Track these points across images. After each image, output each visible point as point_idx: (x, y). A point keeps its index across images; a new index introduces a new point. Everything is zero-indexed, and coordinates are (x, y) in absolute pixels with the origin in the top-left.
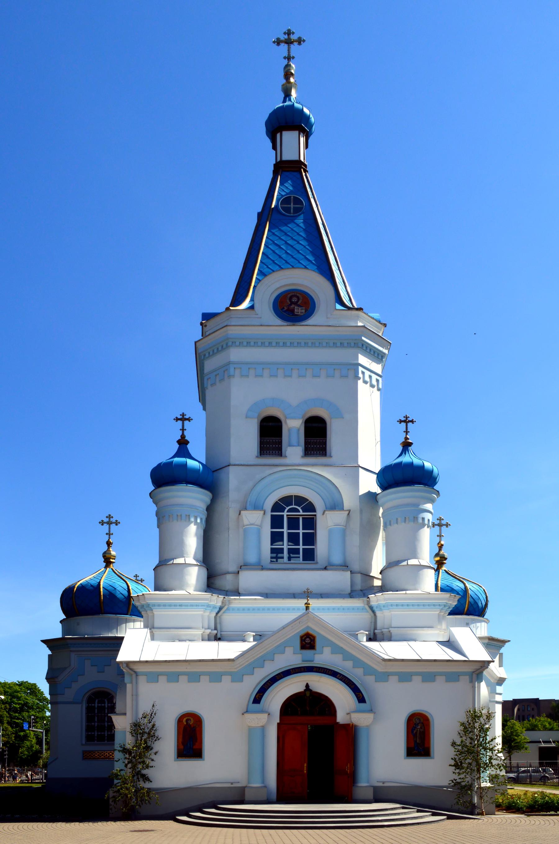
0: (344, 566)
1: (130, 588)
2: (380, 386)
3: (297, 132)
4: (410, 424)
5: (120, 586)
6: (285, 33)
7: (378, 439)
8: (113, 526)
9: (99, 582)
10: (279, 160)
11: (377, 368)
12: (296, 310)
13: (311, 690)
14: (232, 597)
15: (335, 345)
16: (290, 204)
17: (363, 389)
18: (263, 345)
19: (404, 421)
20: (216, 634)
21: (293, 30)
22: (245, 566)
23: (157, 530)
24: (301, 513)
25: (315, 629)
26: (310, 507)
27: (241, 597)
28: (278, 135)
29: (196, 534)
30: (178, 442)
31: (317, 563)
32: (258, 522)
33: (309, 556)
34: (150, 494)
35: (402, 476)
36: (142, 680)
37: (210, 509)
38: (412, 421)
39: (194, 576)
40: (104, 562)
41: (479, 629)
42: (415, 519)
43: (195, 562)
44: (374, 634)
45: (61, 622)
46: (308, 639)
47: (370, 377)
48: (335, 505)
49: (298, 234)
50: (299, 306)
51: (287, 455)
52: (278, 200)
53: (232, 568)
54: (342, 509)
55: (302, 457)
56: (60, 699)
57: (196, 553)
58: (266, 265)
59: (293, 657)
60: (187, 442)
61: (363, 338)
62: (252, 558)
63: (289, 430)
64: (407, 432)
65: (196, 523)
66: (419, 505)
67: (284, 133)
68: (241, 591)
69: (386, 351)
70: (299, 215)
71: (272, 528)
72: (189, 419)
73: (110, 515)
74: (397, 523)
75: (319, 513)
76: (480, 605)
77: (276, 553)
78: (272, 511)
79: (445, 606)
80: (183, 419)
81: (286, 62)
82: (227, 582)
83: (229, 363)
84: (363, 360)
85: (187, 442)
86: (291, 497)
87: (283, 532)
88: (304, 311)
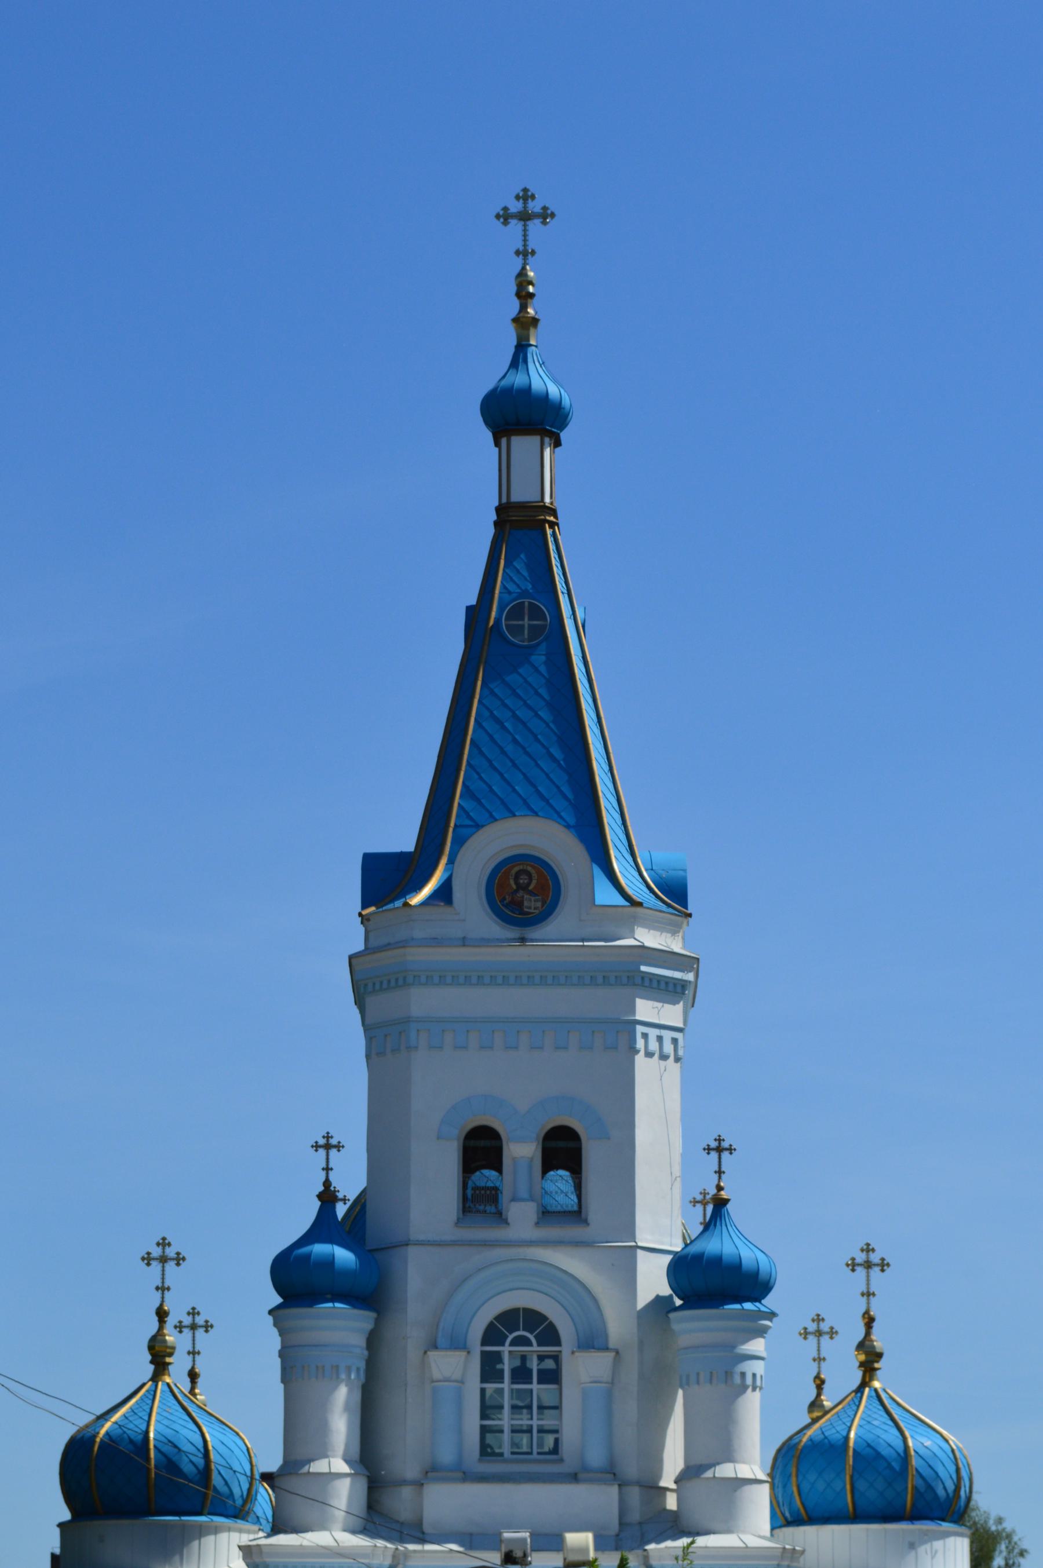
0: (611, 1473)
1: (210, 1448)
3: (536, 440)
5: (187, 1435)
7: (677, 1170)
9: (147, 1432)
11: (671, 1014)
12: (526, 904)
14: (411, 1547)
15: (593, 982)
16: (523, 620)
17: (644, 1068)
18: (467, 981)
22: (433, 1472)
23: (281, 1387)
24: (535, 1347)
26: (550, 1335)
27: (429, 1547)
29: (347, 1408)
30: (320, 1196)
31: (562, 1460)
32: (457, 1375)
35: (715, 1282)
37: (373, 1341)
38: (731, 1150)
39: (344, 1495)
40: (152, 1362)
41: (940, 1555)
42: (728, 1375)
43: (345, 1469)
45: (61, 1525)
47: (660, 1039)
48: (593, 1340)
49: (537, 693)
50: (531, 893)
51: (509, 1220)
52: (501, 609)
53: (411, 1471)
54: (606, 1349)
55: (537, 1224)
57: (347, 1446)
58: (478, 774)
61: (643, 968)
62: (446, 1455)
63: (514, 1159)
65: (349, 1382)
66: (734, 1347)
68: (427, 1528)
69: (690, 977)
70: (538, 644)
72: (339, 1147)
74: (698, 1383)
75: (566, 1348)
76: (941, 1492)
77: (486, 1451)
78: (483, 1344)
80: (328, 1145)
81: (519, 260)
82: (401, 1503)
83: (407, 1020)
84: (645, 1009)
87: (503, 1389)
88: (539, 904)
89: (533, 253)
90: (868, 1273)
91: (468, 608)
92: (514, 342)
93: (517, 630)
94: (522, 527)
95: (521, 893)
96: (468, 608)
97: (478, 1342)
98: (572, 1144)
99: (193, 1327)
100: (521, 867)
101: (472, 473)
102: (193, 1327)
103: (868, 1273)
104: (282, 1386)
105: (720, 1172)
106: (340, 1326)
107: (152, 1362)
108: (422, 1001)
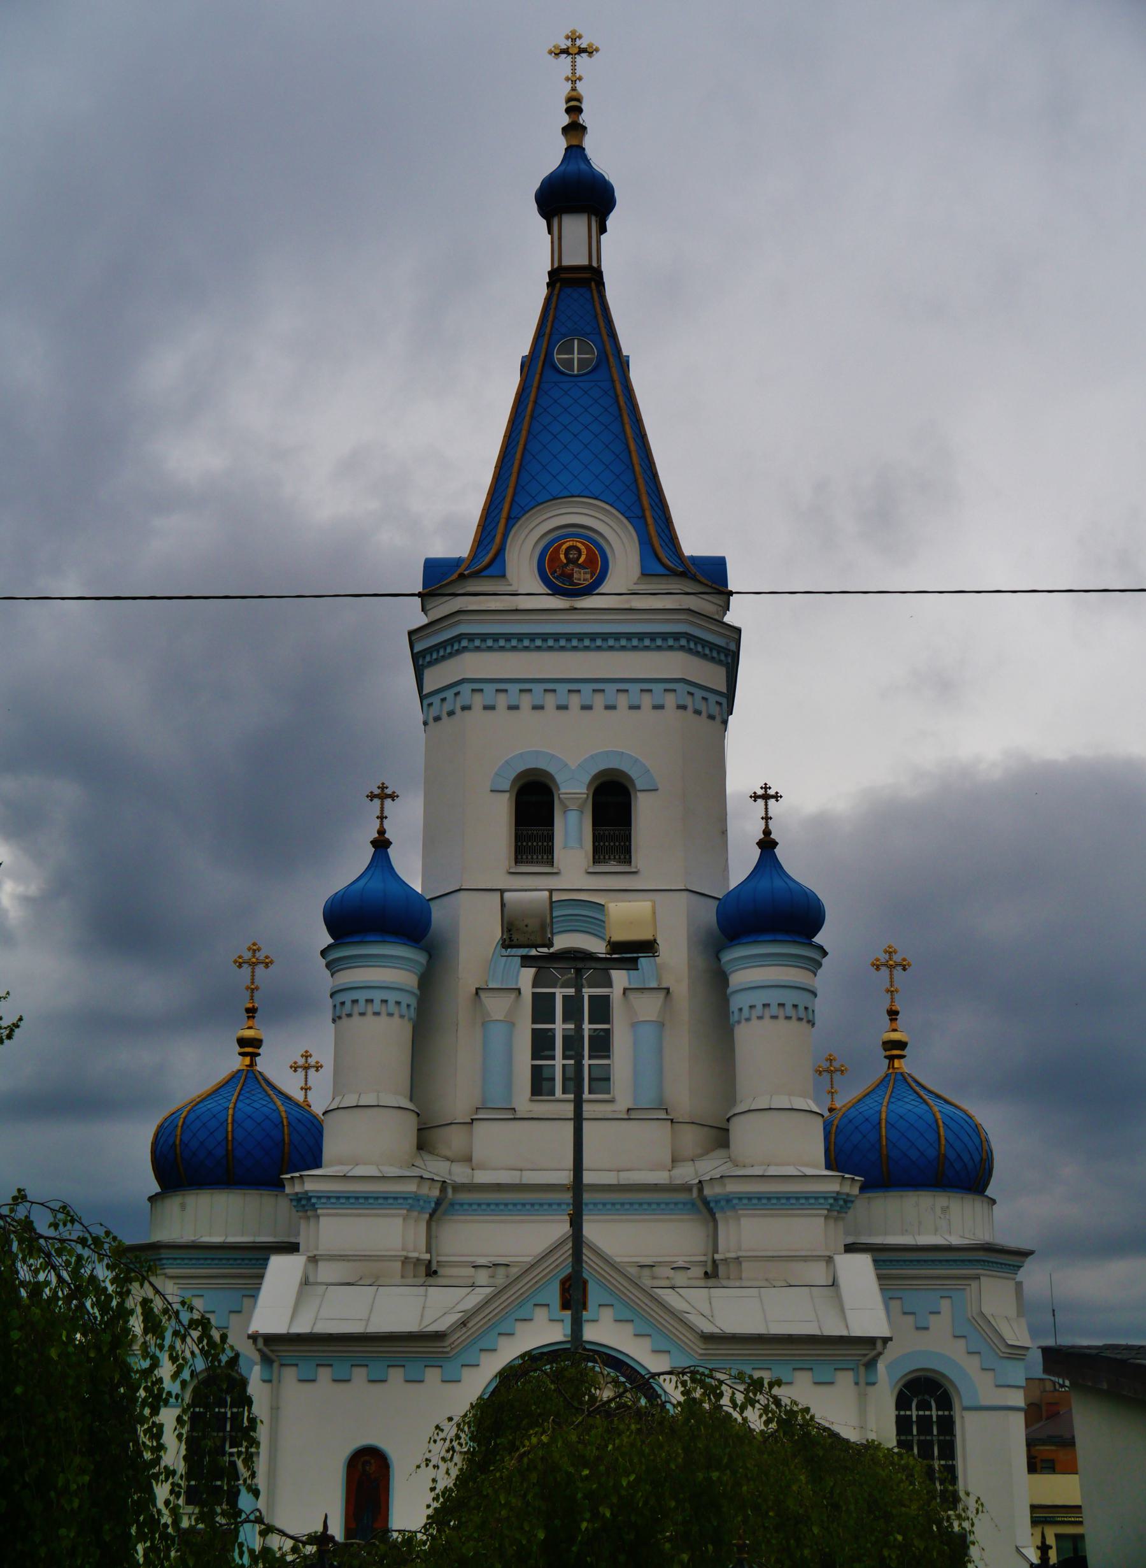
6: (567, 37)
8: (260, 969)
10: (556, 265)
12: (575, 576)
20: (430, 1261)
21: (579, 31)
50: (581, 566)
60: (774, 844)
71: (534, 1022)
77: (540, 1084)
79: (836, 1199)
85: (774, 844)
88: (588, 576)
90: (575, 152)
91: (776, 844)
94: (576, 290)
95: (571, 566)
96: (776, 844)
97: (530, 983)
99: (306, 1068)
100: (571, 543)
101: (529, 253)
102: (306, 1068)
103: (575, 152)
106: (388, 970)
108: (474, 665)
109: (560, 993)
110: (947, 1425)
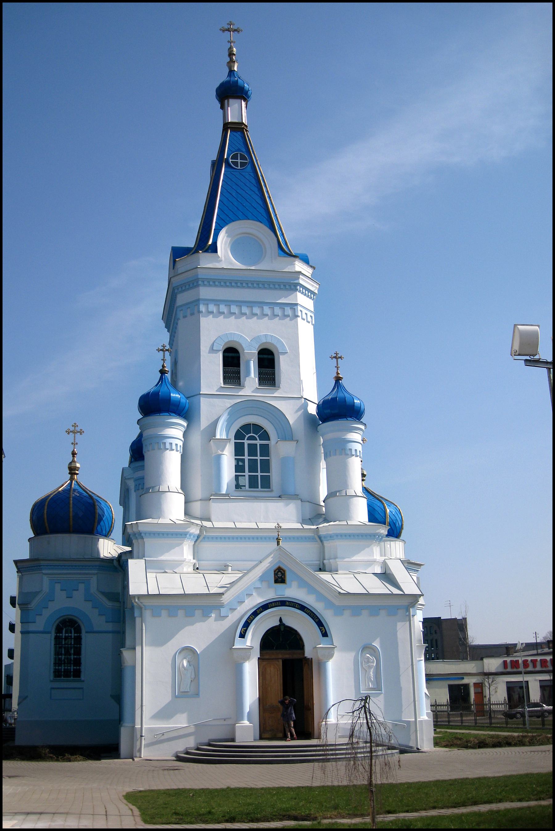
2: (314, 323)
4: (339, 360)
13: (284, 624)
19: (335, 357)
25: (287, 565)
26: (265, 436)
28: (226, 101)
33: (266, 483)
34: (138, 420)
35: (338, 409)
36: (147, 614)
40: (69, 473)
44: (323, 564)
46: (279, 573)
56: (32, 627)
59: (272, 593)
64: (337, 368)
67: (231, 101)
73: (75, 424)
86: (249, 425)
89: (77, 444)
92: (228, 71)
93: (236, 164)
98: (270, 357)
104: (121, 508)
105: (337, 368)
107: (69, 473)
109: (246, 442)
110: (78, 640)
